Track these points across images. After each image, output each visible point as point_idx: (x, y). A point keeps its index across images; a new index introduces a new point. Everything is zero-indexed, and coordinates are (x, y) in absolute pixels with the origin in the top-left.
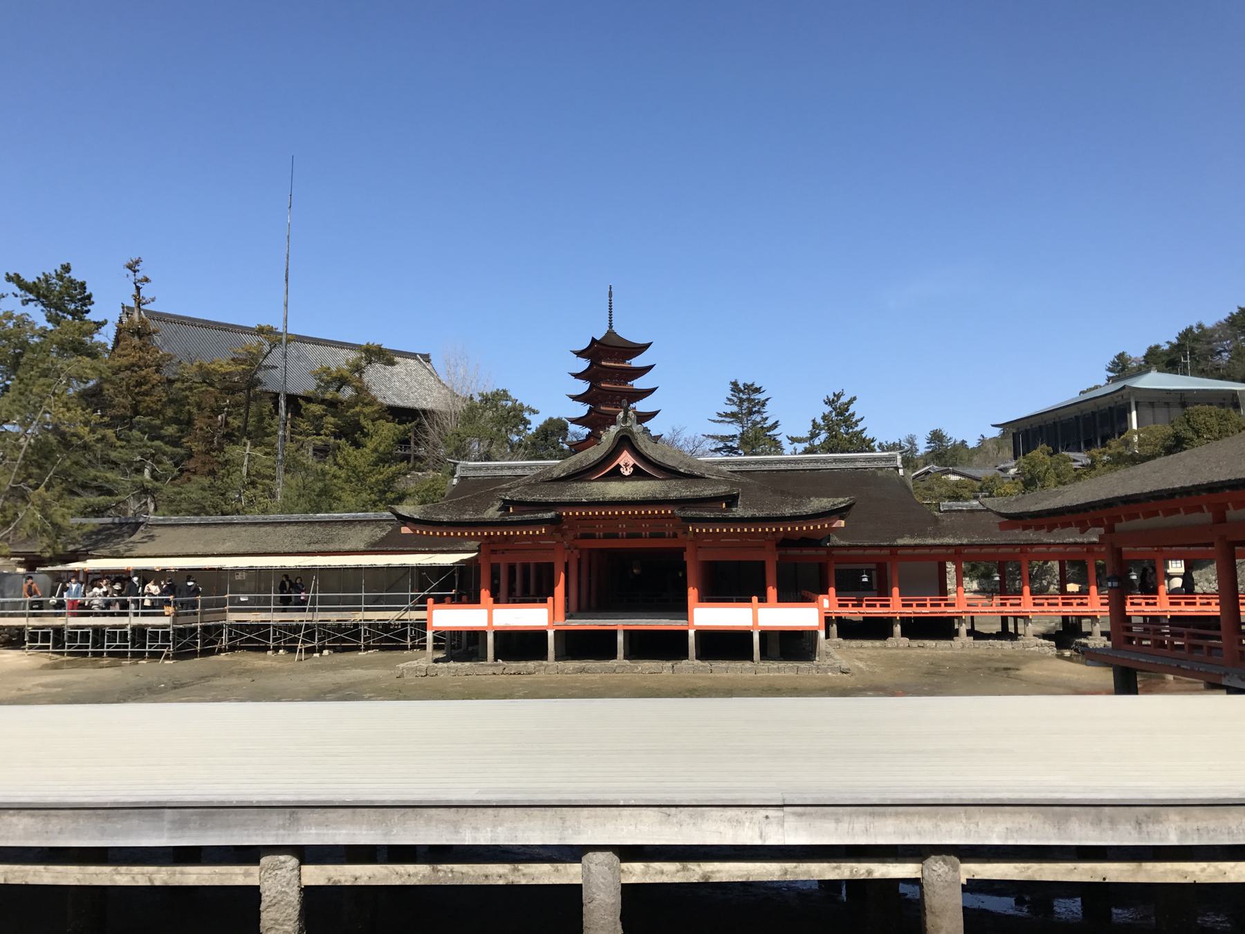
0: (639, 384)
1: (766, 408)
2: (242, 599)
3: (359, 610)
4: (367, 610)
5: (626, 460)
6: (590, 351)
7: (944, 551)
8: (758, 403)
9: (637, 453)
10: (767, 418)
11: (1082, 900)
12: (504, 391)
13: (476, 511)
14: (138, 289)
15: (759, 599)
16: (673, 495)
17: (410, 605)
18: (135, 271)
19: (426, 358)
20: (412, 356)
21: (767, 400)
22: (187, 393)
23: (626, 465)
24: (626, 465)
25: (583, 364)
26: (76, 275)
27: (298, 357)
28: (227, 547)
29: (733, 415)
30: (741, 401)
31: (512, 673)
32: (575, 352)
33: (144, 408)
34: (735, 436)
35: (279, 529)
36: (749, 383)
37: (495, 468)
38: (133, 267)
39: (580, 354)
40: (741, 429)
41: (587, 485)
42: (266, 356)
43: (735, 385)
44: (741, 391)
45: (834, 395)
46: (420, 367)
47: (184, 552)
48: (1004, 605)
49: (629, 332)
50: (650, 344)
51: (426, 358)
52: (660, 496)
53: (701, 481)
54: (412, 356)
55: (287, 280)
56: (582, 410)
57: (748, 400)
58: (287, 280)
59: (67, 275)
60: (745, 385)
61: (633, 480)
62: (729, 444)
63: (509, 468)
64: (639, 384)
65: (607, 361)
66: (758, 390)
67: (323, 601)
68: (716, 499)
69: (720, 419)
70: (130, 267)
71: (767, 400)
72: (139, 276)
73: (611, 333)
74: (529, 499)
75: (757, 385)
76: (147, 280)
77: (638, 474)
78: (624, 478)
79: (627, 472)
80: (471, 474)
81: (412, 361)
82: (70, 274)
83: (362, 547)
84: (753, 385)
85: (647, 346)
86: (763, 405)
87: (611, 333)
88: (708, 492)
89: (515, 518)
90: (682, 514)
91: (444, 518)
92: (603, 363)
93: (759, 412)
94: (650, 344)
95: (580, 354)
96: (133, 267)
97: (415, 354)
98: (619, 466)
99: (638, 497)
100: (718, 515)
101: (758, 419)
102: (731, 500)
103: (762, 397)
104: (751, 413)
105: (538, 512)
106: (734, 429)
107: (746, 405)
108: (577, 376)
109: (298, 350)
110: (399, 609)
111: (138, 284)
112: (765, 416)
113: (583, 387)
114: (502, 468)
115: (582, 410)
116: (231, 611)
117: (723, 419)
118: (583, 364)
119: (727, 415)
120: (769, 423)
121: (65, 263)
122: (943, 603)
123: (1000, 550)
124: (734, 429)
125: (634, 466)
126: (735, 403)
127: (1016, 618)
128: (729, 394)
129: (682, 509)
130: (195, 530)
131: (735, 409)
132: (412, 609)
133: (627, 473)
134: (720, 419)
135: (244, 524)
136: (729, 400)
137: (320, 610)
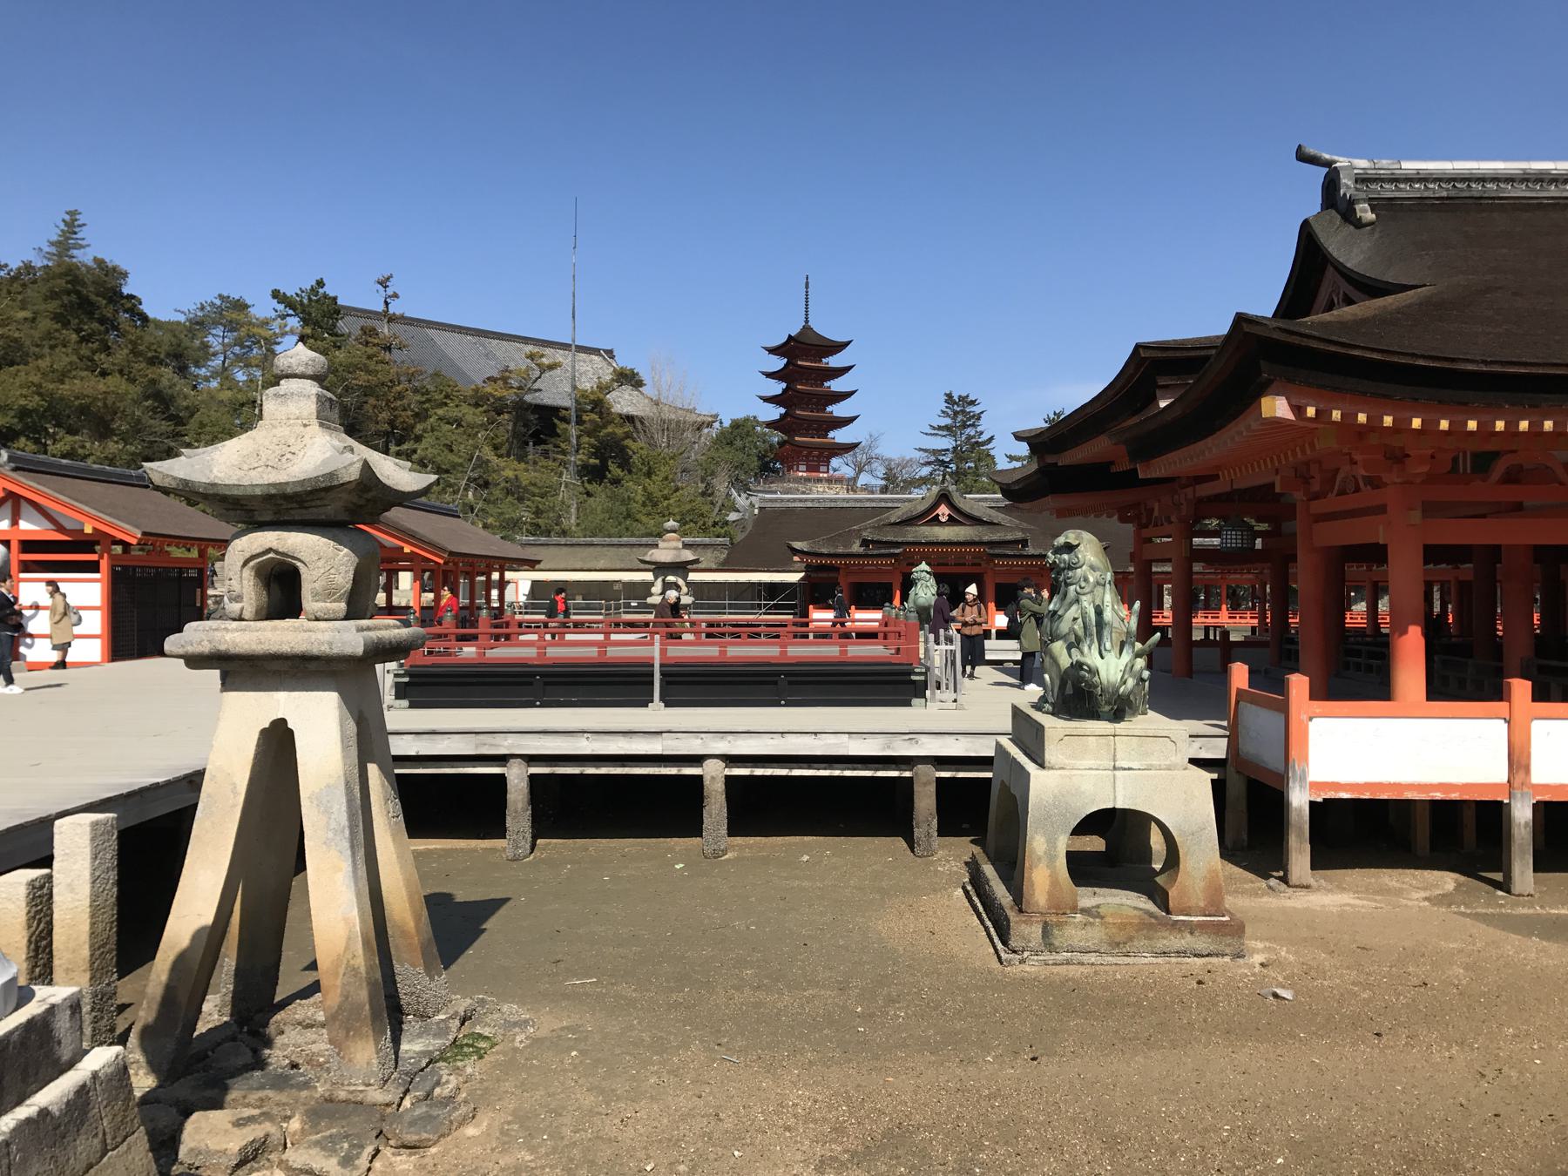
0: (836, 385)
1: (981, 422)
2: (633, 604)
3: (725, 613)
4: (730, 613)
5: (943, 511)
6: (784, 349)
7: (1163, 576)
8: (974, 416)
9: (952, 506)
10: (982, 433)
11: (1191, 635)
12: (755, 417)
13: (845, 546)
14: (387, 304)
15: (224, 678)
16: (986, 538)
17: (763, 610)
18: (386, 287)
19: (610, 353)
20: (596, 351)
21: (982, 412)
22: (427, 405)
23: (943, 514)
24: (943, 514)
25: (778, 363)
26: (330, 290)
27: (487, 355)
28: (601, 565)
29: (947, 428)
30: (956, 413)
31: (424, 1064)
32: (766, 349)
33: (401, 423)
34: (948, 450)
35: (634, 550)
36: (964, 394)
37: (789, 500)
38: (384, 283)
39: (772, 351)
40: (954, 443)
41: (917, 528)
42: (535, 381)
43: (949, 396)
44: (955, 403)
45: (1055, 414)
46: (604, 364)
47: (573, 567)
48: (1207, 617)
49: (827, 329)
50: (849, 342)
51: (610, 353)
52: (977, 539)
53: (997, 527)
54: (596, 351)
55: (574, 317)
56: (775, 413)
57: (963, 412)
58: (574, 317)
59: (321, 291)
60: (960, 396)
61: (948, 525)
62: (941, 458)
63: (800, 500)
64: (838, 410)
65: (803, 360)
66: (973, 403)
67: (731, 606)
68: (1016, 542)
69: (933, 432)
70: (381, 283)
71: (982, 412)
72: (390, 291)
73: (806, 329)
74: (885, 539)
75: (971, 398)
76: (396, 296)
77: (952, 521)
78: (941, 524)
79: (943, 520)
80: (769, 505)
81: (596, 358)
82: (324, 289)
83: (714, 566)
84: (968, 396)
85: (847, 344)
86: (979, 418)
87: (806, 329)
88: (1009, 537)
89: (875, 552)
90: (992, 552)
91: (825, 551)
92: (799, 363)
93: (973, 425)
94: (849, 342)
95: (772, 351)
96: (384, 283)
97: (599, 350)
98: (938, 515)
99: (961, 539)
100: (1016, 552)
101: (972, 433)
102: (1024, 543)
103: (977, 409)
104: (964, 426)
105: (891, 548)
106: (946, 443)
107: (960, 418)
108: (769, 375)
109: (485, 347)
110: (755, 614)
111: (388, 300)
112: (979, 429)
113: (777, 388)
114: (794, 500)
115: (775, 413)
116: (625, 613)
117: (936, 432)
118: (778, 363)
119: (940, 428)
120: (984, 437)
121: (318, 278)
122: (1160, 615)
123: (1206, 577)
124: (946, 443)
125: (949, 515)
126: (948, 415)
127: (1215, 627)
128: (943, 406)
129: (991, 548)
130: (565, 549)
131: (948, 421)
132: (765, 614)
133: (944, 520)
134: (933, 432)
135: (641, 545)
136: (943, 412)
137: (694, 613)
